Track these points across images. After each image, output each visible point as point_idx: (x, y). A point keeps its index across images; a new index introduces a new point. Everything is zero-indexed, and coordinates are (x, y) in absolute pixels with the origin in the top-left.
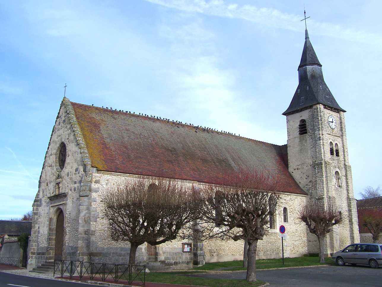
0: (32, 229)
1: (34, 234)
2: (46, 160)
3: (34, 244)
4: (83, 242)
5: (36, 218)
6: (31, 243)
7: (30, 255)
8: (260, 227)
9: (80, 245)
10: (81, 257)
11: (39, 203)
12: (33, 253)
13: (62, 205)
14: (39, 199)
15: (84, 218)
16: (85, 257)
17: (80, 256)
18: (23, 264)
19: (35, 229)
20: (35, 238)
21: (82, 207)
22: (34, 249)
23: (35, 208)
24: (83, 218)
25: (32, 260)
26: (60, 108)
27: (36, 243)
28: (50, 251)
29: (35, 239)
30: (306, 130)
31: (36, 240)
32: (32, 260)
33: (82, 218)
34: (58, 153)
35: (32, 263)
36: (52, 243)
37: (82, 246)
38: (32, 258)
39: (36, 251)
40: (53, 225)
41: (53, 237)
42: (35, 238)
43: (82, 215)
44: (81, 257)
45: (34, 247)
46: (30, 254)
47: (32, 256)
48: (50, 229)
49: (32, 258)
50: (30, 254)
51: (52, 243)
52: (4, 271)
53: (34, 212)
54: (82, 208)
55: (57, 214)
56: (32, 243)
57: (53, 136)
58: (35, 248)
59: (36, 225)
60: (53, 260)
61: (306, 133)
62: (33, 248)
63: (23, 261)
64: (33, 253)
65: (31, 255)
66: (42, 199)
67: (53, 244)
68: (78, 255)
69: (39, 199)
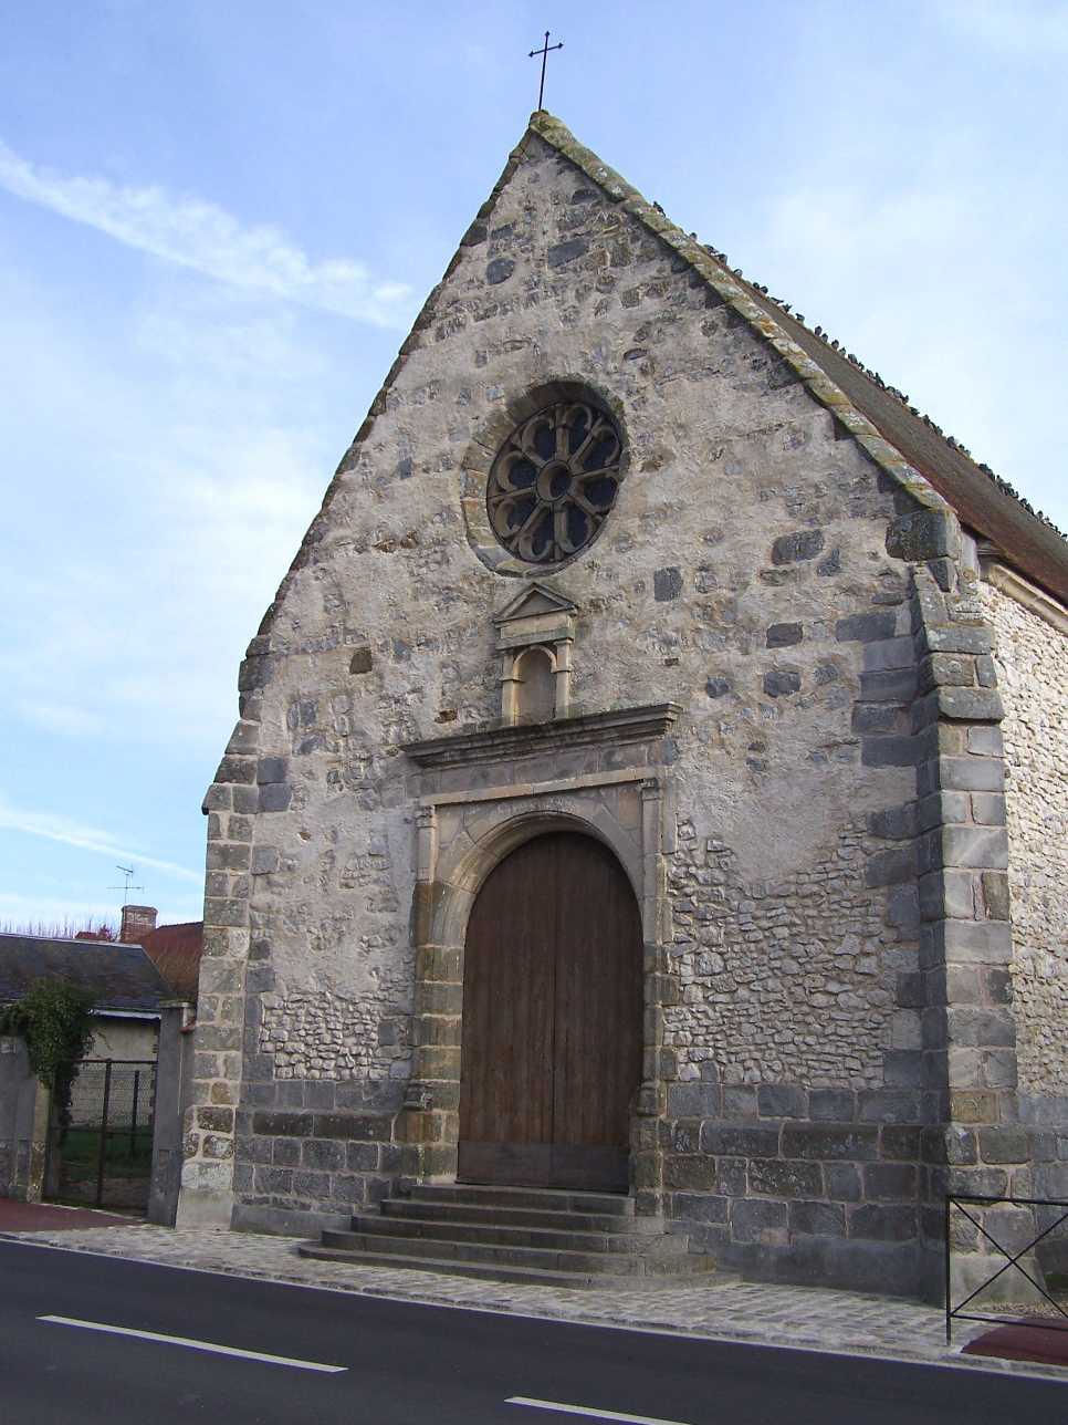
0: (208, 959)
1: (217, 989)
2: (332, 507)
3: (221, 1055)
4: (987, 1055)
5: (229, 887)
6: (196, 1052)
7: (197, 1130)
8: (345, 628)
9: (962, 1075)
10: (981, 1166)
11: (255, 785)
12: (214, 1120)
13: (583, 794)
14: (251, 758)
15: (977, 879)
16: (1010, 1169)
17: (972, 1161)
18: (45, 1181)
19: (227, 958)
20: (226, 1015)
21: (961, 795)
22: (220, 1093)
23: (224, 817)
24: (976, 876)
25: (209, 1165)
26: (506, 178)
27: (233, 1053)
28: (436, 1111)
29: (228, 1024)
31: (232, 1032)
32: (209, 1165)
33: (965, 877)
34: (487, 455)
35: (212, 1184)
36: (441, 1055)
37: (975, 1084)
38: (206, 1153)
39: (234, 1108)
40: (449, 931)
41: (447, 1018)
42: (226, 1015)
43: (966, 855)
44: (981, 1166)
45: (220, 1080)
46: (195, 1124)
47: (207, 1140)
48: (422, 961)
49: (206, 1153)
50: (195, 1124)
51: (441, 1055)
52: (23, 1237)
53: (221, 843)
54: (958, 802)
55: (493, 859)
56: (201, 1047)
57: (416, 354)
58: (227, 1081)
59: (233, 932)
60: (452, 1172)
62: (212, 1081)
63: (48, 1161)
64: (214, 1120)
65: (203, 1134)
66: (295, 762)
67: (448, 1062)
68: (955, 1153)
69: (251, 758)
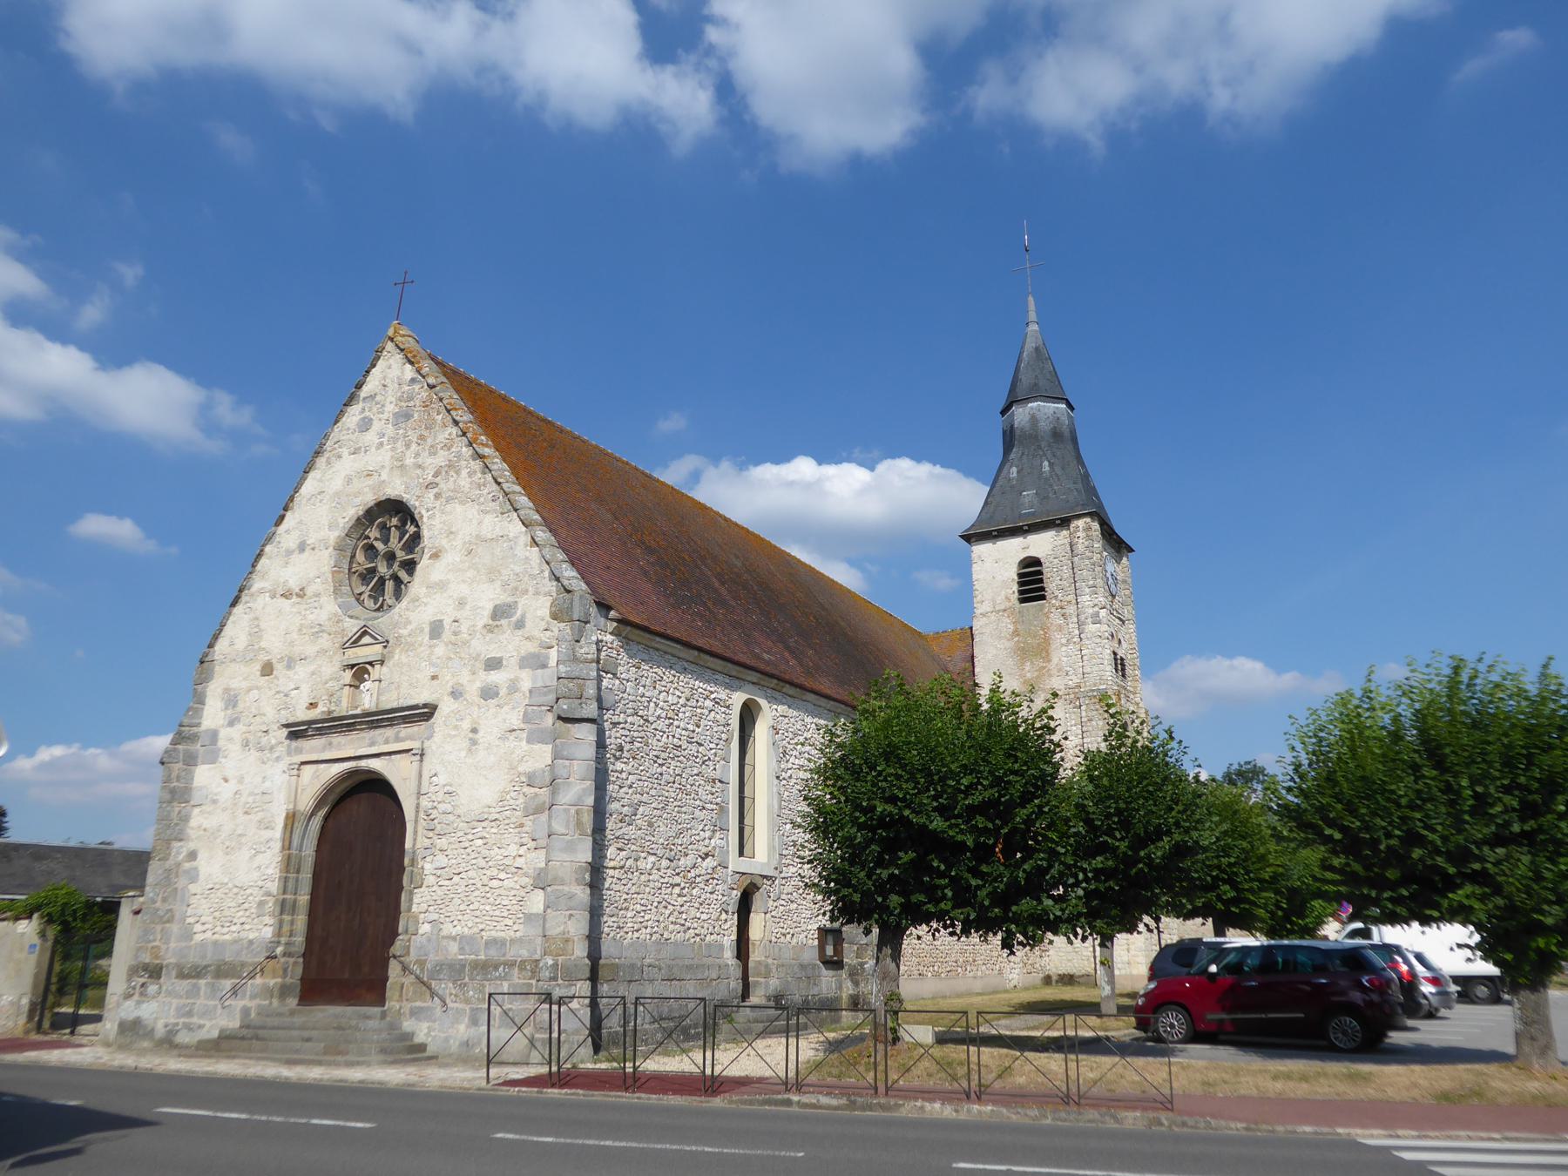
24: (573, 810)
30: (1043, 589)
43: (567, 798)
61: (1043, 598)
